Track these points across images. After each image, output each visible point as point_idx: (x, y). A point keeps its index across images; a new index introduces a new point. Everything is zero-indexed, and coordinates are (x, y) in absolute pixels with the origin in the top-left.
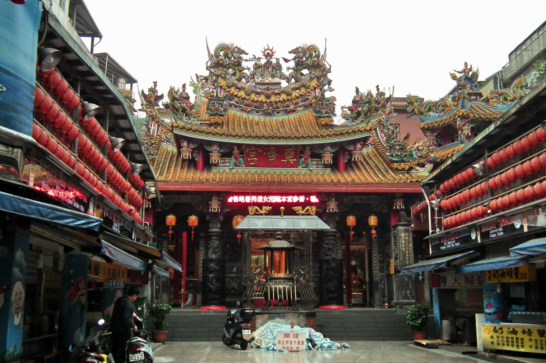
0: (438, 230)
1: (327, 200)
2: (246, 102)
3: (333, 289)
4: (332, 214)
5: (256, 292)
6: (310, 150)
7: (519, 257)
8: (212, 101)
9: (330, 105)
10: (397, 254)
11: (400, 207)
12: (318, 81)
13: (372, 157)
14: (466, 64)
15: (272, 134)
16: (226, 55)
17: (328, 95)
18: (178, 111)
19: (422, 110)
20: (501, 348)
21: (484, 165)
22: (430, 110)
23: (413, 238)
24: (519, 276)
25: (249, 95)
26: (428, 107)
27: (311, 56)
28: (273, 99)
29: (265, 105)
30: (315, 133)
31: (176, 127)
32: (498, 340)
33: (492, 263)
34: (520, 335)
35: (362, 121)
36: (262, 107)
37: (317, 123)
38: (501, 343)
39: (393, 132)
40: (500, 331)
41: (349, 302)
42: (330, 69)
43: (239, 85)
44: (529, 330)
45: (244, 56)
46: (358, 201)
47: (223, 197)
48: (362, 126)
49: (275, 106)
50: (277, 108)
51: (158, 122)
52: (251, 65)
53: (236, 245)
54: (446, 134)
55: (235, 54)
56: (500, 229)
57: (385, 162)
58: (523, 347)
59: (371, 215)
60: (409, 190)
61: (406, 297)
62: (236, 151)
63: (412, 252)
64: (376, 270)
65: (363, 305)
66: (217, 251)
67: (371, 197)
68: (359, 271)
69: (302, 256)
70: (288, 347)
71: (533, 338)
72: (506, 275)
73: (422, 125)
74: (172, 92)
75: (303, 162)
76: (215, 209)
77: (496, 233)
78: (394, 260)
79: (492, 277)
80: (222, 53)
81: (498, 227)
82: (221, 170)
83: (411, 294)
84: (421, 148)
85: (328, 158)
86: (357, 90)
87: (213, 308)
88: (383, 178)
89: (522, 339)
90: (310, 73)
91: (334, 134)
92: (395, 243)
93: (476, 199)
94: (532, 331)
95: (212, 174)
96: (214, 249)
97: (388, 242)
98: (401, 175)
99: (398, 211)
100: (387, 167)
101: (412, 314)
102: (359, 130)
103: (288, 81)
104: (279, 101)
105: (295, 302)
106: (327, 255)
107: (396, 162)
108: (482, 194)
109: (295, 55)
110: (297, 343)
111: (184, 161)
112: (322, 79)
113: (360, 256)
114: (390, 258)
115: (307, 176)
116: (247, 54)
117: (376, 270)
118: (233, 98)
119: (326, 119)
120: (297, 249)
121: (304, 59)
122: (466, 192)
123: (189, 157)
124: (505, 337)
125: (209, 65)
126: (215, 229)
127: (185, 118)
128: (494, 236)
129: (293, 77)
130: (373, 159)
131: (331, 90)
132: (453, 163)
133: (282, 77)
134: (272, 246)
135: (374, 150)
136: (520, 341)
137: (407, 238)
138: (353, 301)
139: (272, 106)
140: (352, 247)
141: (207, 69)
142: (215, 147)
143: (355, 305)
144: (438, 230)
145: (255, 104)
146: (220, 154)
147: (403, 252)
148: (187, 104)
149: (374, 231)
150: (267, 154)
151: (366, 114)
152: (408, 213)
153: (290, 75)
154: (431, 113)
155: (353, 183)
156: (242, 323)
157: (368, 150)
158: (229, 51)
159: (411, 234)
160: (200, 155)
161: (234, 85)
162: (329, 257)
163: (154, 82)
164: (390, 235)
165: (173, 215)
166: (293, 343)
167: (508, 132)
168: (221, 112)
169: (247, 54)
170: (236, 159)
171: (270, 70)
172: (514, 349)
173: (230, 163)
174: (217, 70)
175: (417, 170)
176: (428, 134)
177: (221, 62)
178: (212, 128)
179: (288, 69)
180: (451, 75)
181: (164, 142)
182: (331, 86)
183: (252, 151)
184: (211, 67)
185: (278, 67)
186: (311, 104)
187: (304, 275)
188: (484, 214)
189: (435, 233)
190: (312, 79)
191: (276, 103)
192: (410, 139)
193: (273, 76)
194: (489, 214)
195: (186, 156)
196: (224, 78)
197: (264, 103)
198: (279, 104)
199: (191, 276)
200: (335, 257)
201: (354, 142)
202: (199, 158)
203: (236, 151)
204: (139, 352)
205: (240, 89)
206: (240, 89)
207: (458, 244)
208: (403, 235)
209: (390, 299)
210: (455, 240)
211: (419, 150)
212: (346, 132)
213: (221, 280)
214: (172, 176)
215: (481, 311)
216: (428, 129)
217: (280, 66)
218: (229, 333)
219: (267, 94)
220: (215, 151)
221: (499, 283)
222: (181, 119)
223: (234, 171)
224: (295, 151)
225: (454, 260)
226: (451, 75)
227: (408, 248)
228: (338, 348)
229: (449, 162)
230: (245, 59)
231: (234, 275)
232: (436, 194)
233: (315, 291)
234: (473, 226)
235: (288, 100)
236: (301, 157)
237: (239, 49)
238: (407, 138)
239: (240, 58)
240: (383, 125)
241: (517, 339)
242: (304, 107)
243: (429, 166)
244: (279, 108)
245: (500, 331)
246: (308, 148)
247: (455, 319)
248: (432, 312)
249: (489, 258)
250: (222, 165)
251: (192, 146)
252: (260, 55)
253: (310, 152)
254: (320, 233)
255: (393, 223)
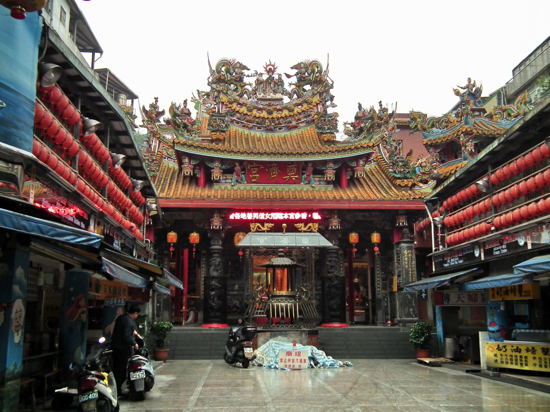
0: (441, 247)
1: (329, 216)
2: (248, 118)
3: (335, 307)
4: (334, 231)
5: (258, 309)
6: (312, 166)
7: (523, 274)
8: (213, 117)
9: (332, 121)
10: (400, 272)
11: (403, 223)
12: (320, 97)
13: (375, 173)
14: (469, 80)
15: (274, 150)
16: (228, 71)
17: (330, 111)
18: (179, 127)
19: (426, 126)
20: (504, 366)
21: (488, 182)
22: (433, 126)
23: (416, 255)
24: (523, 294)
25: (251, 111)
26: (431, 123)
27: (313, 71)
28: (275, 115)
29: (267, 121)
30: (317, 149)
31: (177, 143)
32: (501, 359)
33: (496, 280)
34: (524, 353)
35: (365, 138)
36: (264, 123)
37: (319, 139)
38: (504, 361)
39: (396, 148)
40: (504, 349)
41: (352, 319)
42: (332, 85)
43: (241, 101)
44: (533, 348)
45: (246, 72)
46: (361, 218)
47: (224, 214)
48: (365, 142)
49: (277, 122)
50: (279, 124)
51: (159, 138)
52: (253, 80)
53: (238, 263)
54: (449, 150)
55: (236, 70)
56: (504, 246)
57: (388, 178)
58: (526, 365)
59: (374, 232)
60: (412, 206)
61: (409, 315)
62: (238, 168)
63: (415, 269)
64: (379, 288)
65: (365, 323)
66: (218, 268)
67: (374, 214)
68: (362, 288)
69: (304, 273)
70: (290, 366)
71: (537, 356)
72: (510, 292)
73: (425, 141)
74: (173, 108)
75: (305, 179)
76: (216, 226)
77: (499, 250)
78: (396, 277)
79: (496, 295)
80: (223, 69)
81: (501, 244)
82: (223, 187)
83: (414, 311)
84: (424, 164)
85: (330, 175)
86: (360, 106)
87: (215, 325)
88: (385, 195)
89: (526, 357)
90: (312, 89)
91: (336, 151)
92: (397, 260)
93: (480, 216)
94: (536, 349)
95: (213, 191)
96: (215, 266)
97: (391, 259)
98: (403, 192)
99: (401, 228)
100: (390, 184)
101: (415, 332)
102: (361, 146)
103: (291, 97)
104: (281, 117)
105: (298, 320)
106: (329, 273)
107: (399, 178)
108: (485, 211)
109: (297, 71)
110: (299, 361)
111: (185, 177)
112: (324, 94)
113: (362, 274)
114: (393, 275)
115: (309, 193)
116: (249, 70)
117: (379, 288)
118: (235, 114)
119: (329, 135)
120: (299, 266)
121: (306, 74)
122: (469, 209)
123: (190, 174)
124: (509, 355)
125: (210, 80)
126: (217, 246)
127: (186, 134)
128: (497, 253)
129: (295, 92)
130: (376, 175)
131: (334, 106)
132: (456, 179)
133: (284, 92)
134: (274, 264)
135: (377, 167)
136: (523, 359)
137: (410, 255)
138: (356, 319)
139: (274, 122)
140: (355, 265)
141: (208, 85)
142: (217, 164)
143: (357, 323)
144: (441, 247)
145: (257, 120)
146: (221, 171)
147: (406, 269)
148: (188, 120)
149: (376, 249)
150: (269, 170)
151: (368, 130)
152: (411, 230)
153: (292, 91)
154: (434, 129)
155: (356, 200)
156: (244, 341)
157: (371, 167)
158: (231, 67)
159: (414, 251)
160: (202, 171)
161: (235, 101)
162: (331, 275)
163: (155, 98)
164: (393, 252)
165: (174, 232)
166: (295, 361)
167: (512, 148)
168: (223, 128)
169: (249, 70)
170: (238, 175)
171: (272, 85)
172: (518, 367)
173: (231, 179)
174: (218, 86)
175: (420, 187)
176: (431, 150)
177: (222, 78)
178: (214, 144)
179: (290, 84)
180: (455, 90)
181: (165, 158)
182: (333, 102)
183: (253, 167)
184: (213, 82)
185: (280, 83)
186: (314, 120)
187: (307, 293)
188: (488, 231)
189: (439, 250)
190: (314, 95)
191: (278, 119)
192: (413, 155)
193: (275, 92)
194: (492, 232)
195: (187, 173)
196: (226, 94)
197: (266, 119)
198: (281, 120)
199: (192, 294)
200: (338, 274)
201: (357, 159)
202: (200, 175)
203: (238, 168)
204: (140, 370)
205: (241, 105)
206: (241, 105)
207: (461, 261)
208: (406, 252)
209: (393, 316)
210: (459, 257)
211: (422, 167)
212: (349, 149)
213: (223, 297)
214: (173, 193)
215: (485, 329)
216: (431, 145)
217: (282, 82)
218: (231, 351)
219: (269, 110)
220: (217, 167)
221: (503, 300)
222: (182, 135)
223: (236, 188)
224: (298, 168)
225: (457, 277)
226: (455, 90)
227: (412, 265)
228: (341, 366)
229: (452, 178)
230: (247, 75)
231: (235, 293)
232: (439, 211)
233: (318, 309)
234: (506, 233)
235: (290, 116)
236: (303, 174)
237: (241, 65)
238: (410, 154)
239: (242, 74)
240: (386, 141)
241: (521, 357)
242: (307, 123)
243: (432, 183)
244: (281, 124)
245: (504, 349)
246: (310, 165)
247: (458, 337)
248: (435, 330)
249: (493, 276)
250: (224, 181)
251: (193, 163)
252: (262, 70)
253: (312, 168)
254: (323, 250)
255: (396, 240)
